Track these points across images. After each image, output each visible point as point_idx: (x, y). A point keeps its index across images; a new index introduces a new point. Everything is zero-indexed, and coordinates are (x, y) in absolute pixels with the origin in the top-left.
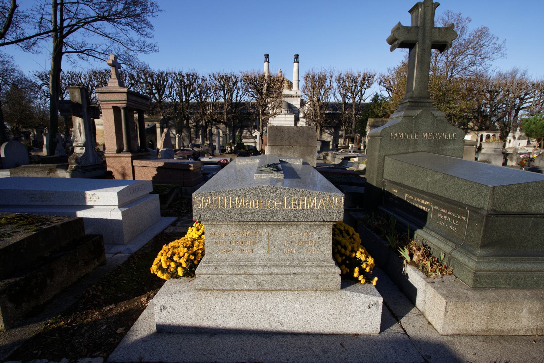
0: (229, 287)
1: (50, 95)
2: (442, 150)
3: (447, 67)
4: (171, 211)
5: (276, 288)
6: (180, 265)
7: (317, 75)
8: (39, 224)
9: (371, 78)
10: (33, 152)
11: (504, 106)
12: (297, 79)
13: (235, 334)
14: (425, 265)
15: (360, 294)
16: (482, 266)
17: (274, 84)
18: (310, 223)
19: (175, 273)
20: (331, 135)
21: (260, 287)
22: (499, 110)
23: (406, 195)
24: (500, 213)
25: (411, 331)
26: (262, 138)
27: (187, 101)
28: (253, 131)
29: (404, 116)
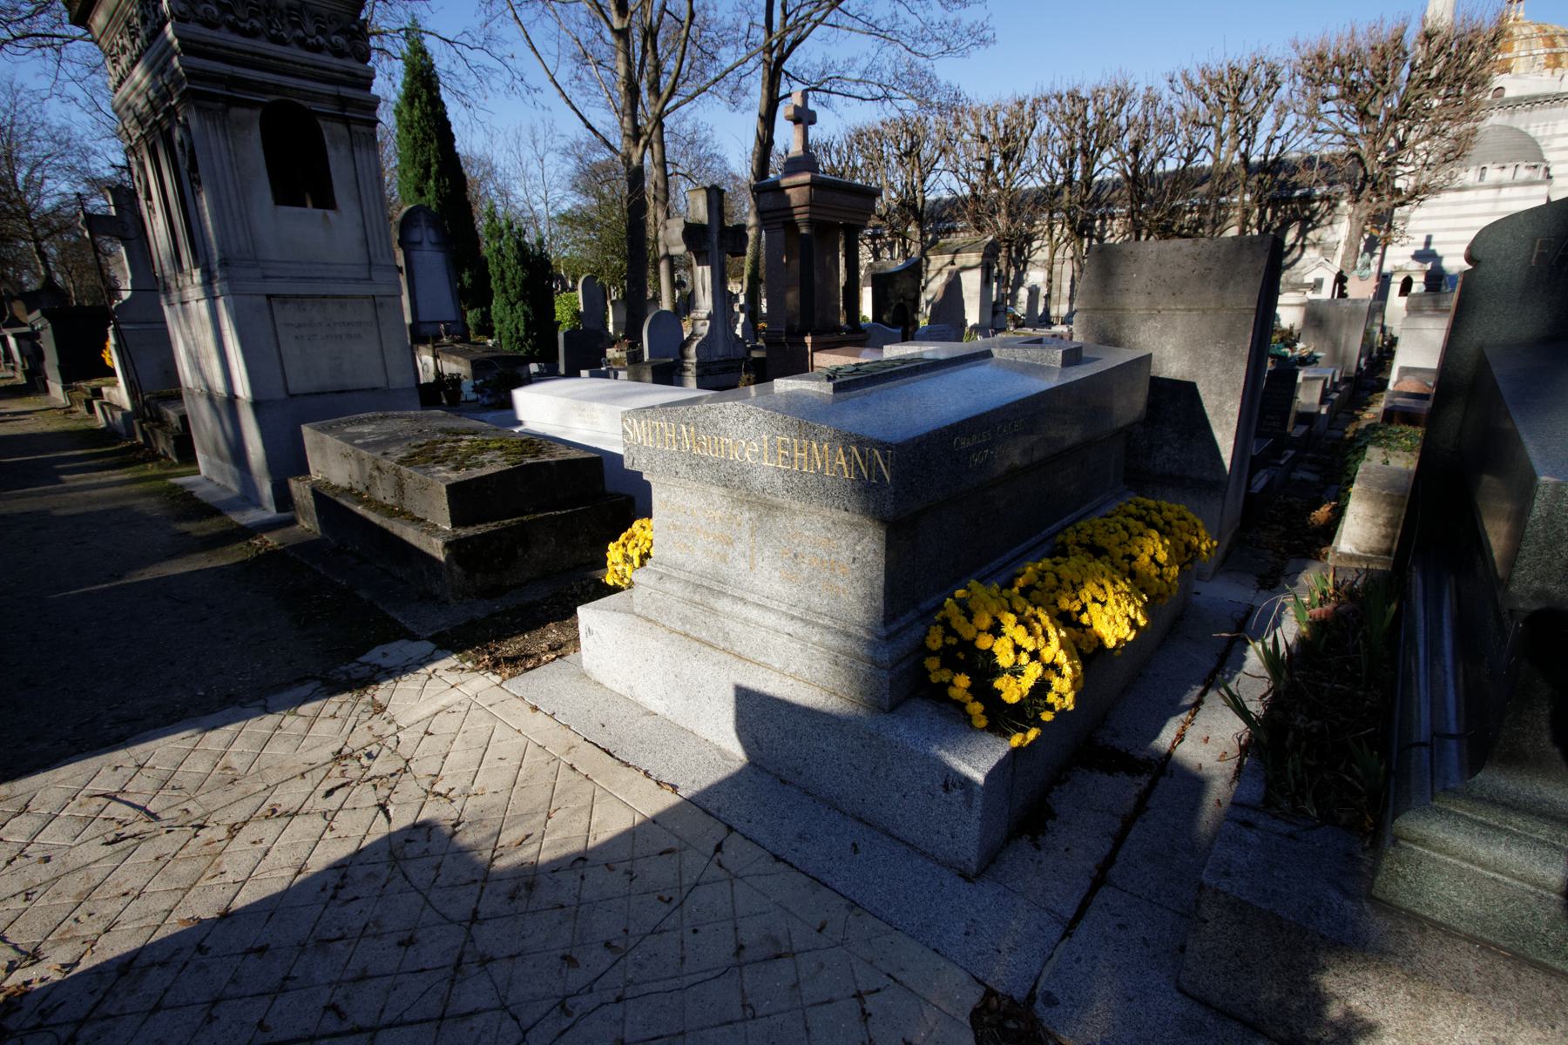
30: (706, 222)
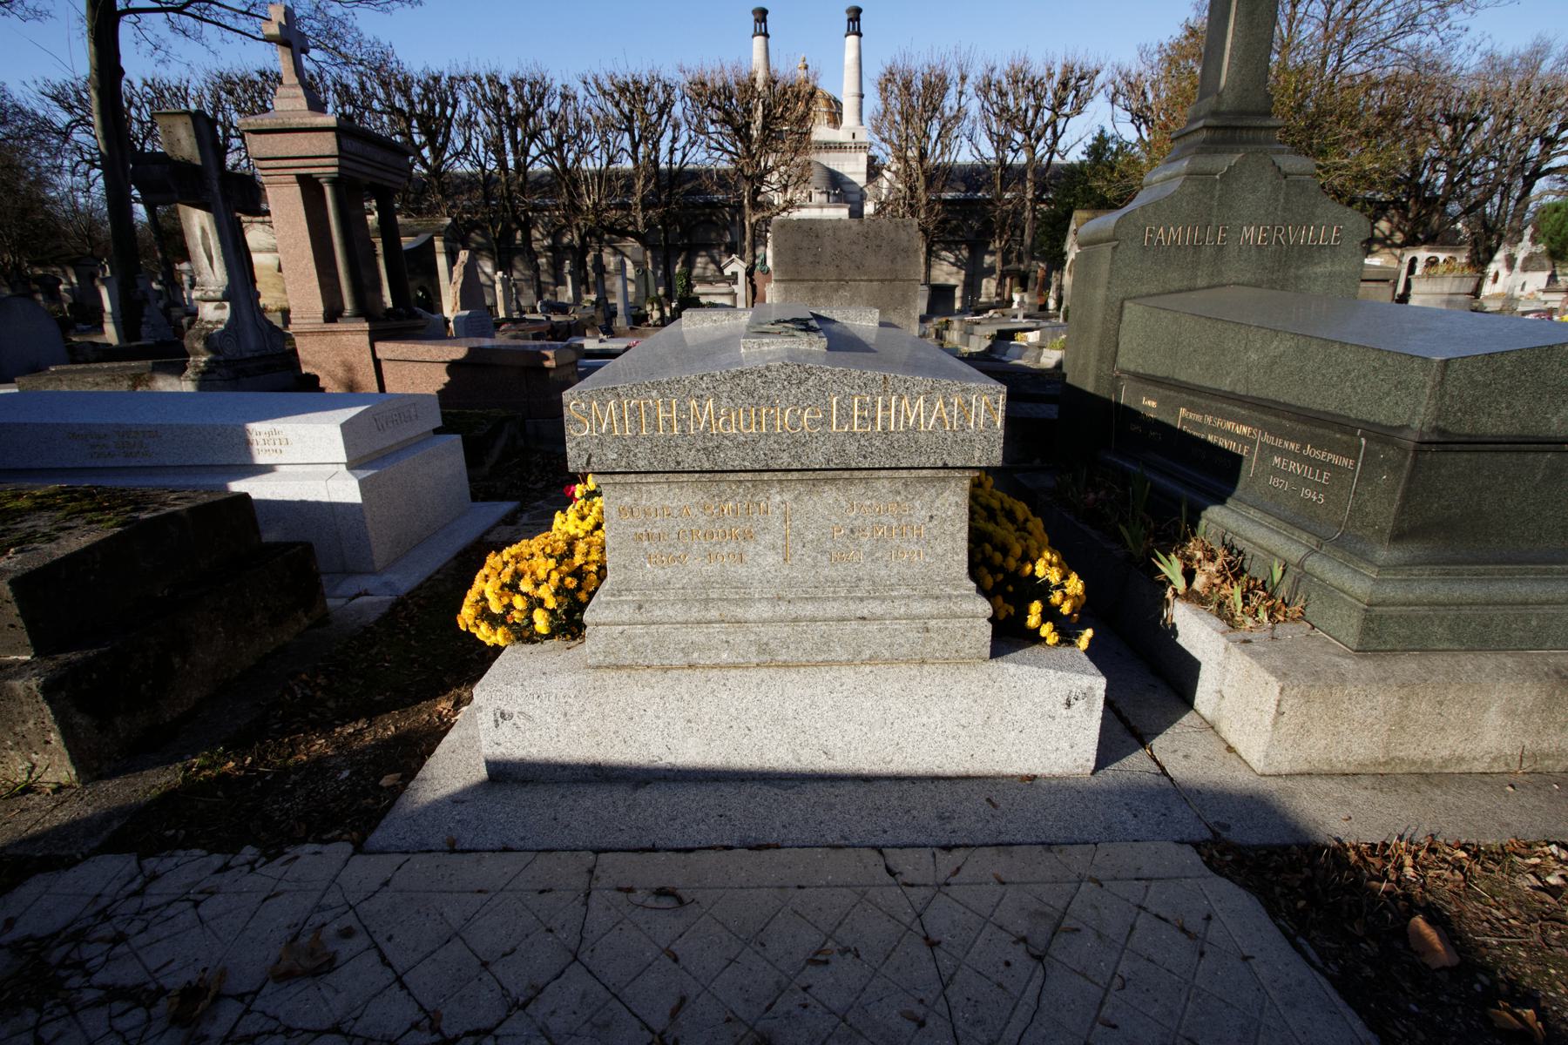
0: (678, 660)
1: (101, 153)
2: (1297, 278)
3: (1328, 37)
4: (498, 484)
5: (810, 658)
6: (541, 603)
7: (919, 74)
8: (128, 508)
9: (1085, 81)
10: (75, 335)
11: (1491, 165)
12: (855, 90)
13: (701, 781)
14: (1227, 597)
15: (1044, 670)
16: (1389, 592)
17: (786, 109)
18: (905, 473)
19: (528, 626)
20: (960, 267)
21: (767, 658)
22: (1475, 181)
23: (1183, 411)
24: (1456, 439)
25: (1179, 768)
26: (752, 281)
27: (521, 167)
28: (725, 261)
29: (1190, 174)
30: (199, 162)
